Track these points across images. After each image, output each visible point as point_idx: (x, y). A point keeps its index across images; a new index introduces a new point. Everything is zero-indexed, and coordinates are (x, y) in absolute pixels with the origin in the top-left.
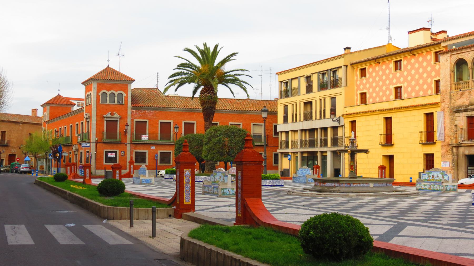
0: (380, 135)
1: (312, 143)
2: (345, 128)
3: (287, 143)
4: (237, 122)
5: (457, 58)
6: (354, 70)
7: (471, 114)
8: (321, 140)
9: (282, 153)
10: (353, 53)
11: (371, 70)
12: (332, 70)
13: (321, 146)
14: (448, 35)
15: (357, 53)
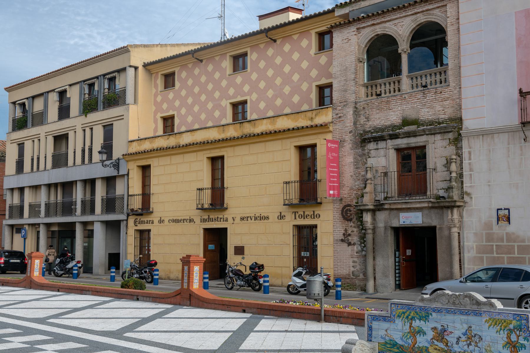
0: (199, 189)
3: (21, 208)
5: (372, 33)
6: (152, 75)
7: (408, 144)
8: (83, 202)
9: (12, 226)
11: (184, 74)
12: (107, 76)
14: (313, 54)
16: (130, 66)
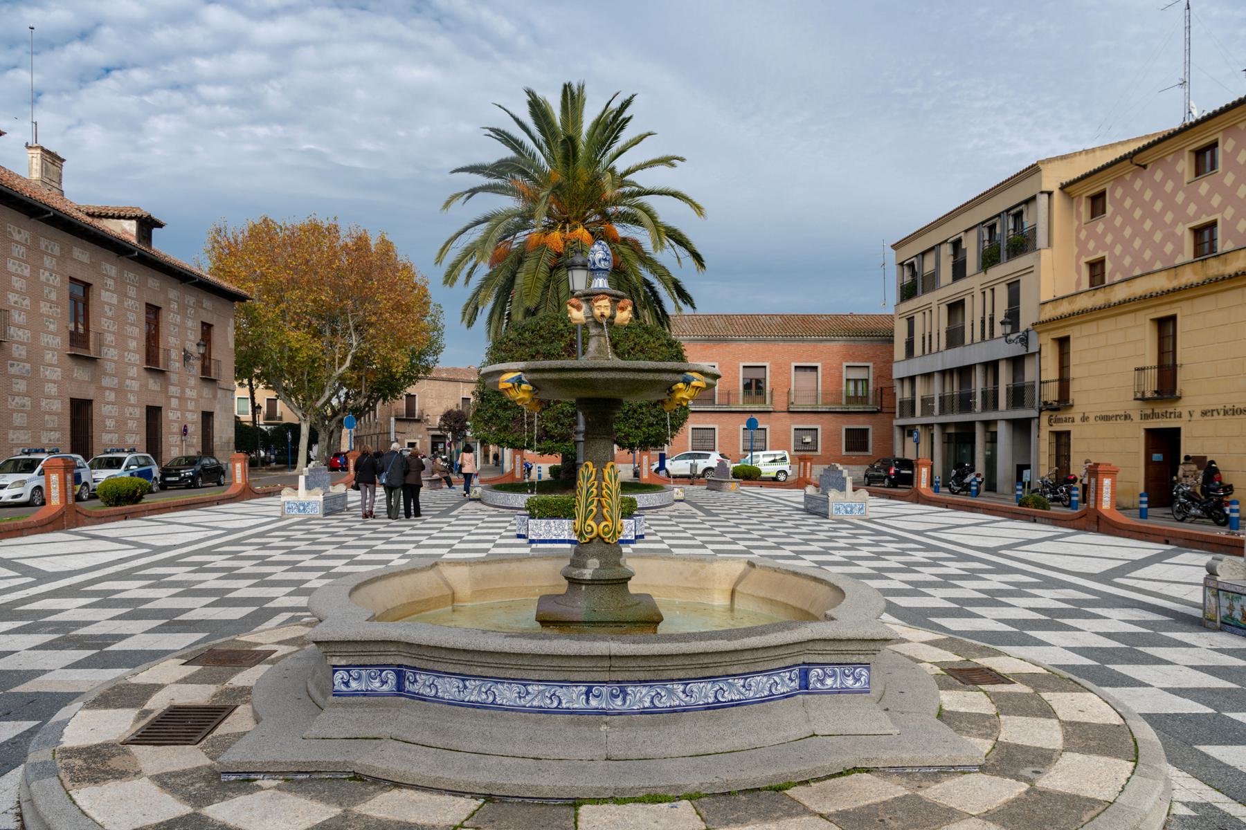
1: (965, 403)
2: (1042, 360)
4: (810, 361)
8: (984, 394)
9: (903, 427)
10: (1072, 157)
12: (1012, 212)
13: (985, 408)
15: (1083, 156)
16: (1042, 192)
